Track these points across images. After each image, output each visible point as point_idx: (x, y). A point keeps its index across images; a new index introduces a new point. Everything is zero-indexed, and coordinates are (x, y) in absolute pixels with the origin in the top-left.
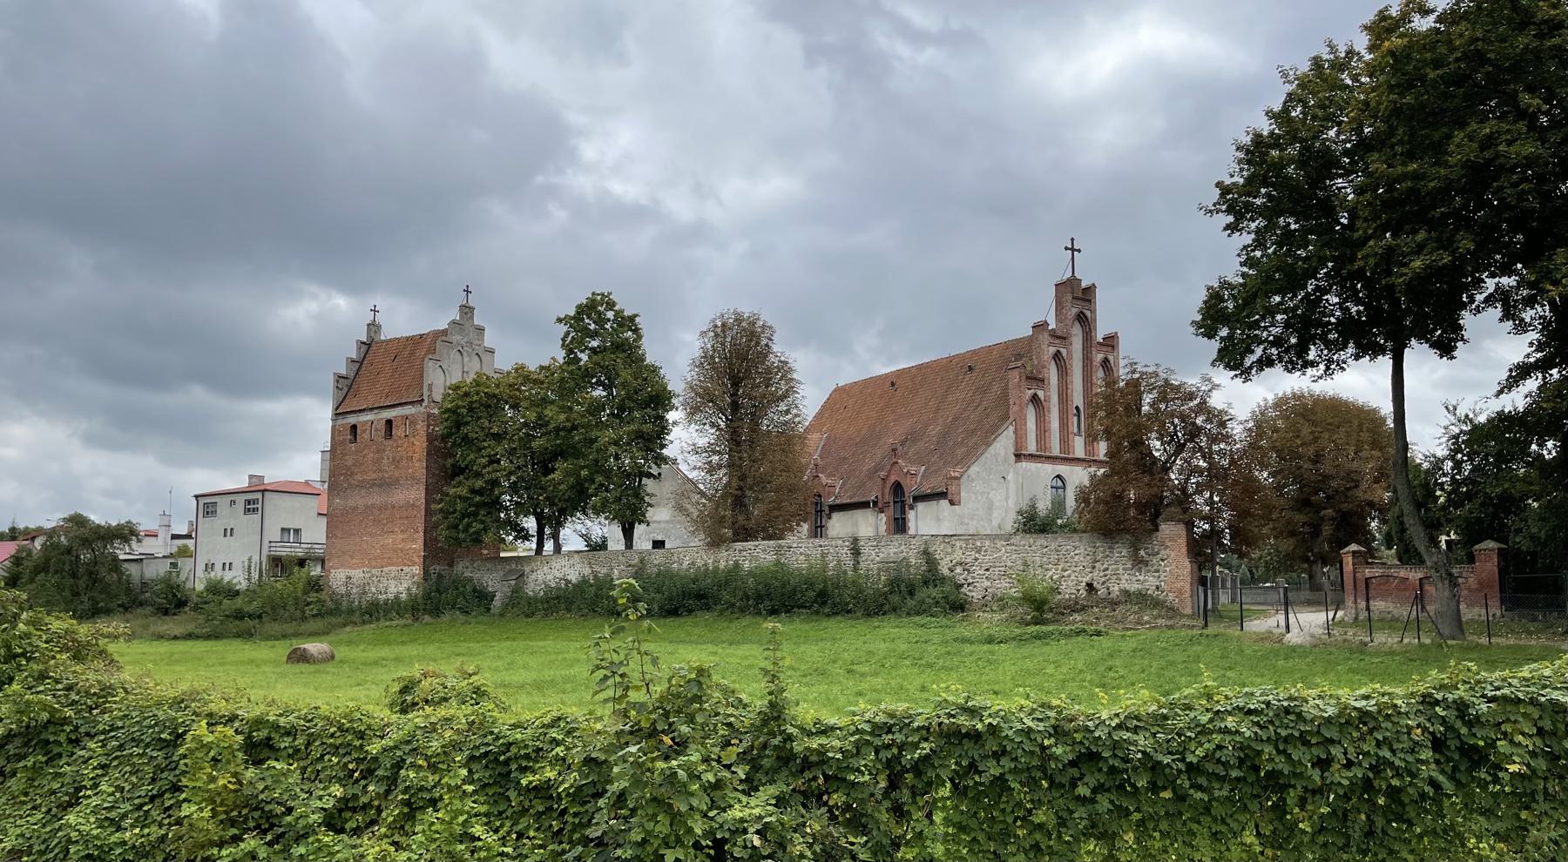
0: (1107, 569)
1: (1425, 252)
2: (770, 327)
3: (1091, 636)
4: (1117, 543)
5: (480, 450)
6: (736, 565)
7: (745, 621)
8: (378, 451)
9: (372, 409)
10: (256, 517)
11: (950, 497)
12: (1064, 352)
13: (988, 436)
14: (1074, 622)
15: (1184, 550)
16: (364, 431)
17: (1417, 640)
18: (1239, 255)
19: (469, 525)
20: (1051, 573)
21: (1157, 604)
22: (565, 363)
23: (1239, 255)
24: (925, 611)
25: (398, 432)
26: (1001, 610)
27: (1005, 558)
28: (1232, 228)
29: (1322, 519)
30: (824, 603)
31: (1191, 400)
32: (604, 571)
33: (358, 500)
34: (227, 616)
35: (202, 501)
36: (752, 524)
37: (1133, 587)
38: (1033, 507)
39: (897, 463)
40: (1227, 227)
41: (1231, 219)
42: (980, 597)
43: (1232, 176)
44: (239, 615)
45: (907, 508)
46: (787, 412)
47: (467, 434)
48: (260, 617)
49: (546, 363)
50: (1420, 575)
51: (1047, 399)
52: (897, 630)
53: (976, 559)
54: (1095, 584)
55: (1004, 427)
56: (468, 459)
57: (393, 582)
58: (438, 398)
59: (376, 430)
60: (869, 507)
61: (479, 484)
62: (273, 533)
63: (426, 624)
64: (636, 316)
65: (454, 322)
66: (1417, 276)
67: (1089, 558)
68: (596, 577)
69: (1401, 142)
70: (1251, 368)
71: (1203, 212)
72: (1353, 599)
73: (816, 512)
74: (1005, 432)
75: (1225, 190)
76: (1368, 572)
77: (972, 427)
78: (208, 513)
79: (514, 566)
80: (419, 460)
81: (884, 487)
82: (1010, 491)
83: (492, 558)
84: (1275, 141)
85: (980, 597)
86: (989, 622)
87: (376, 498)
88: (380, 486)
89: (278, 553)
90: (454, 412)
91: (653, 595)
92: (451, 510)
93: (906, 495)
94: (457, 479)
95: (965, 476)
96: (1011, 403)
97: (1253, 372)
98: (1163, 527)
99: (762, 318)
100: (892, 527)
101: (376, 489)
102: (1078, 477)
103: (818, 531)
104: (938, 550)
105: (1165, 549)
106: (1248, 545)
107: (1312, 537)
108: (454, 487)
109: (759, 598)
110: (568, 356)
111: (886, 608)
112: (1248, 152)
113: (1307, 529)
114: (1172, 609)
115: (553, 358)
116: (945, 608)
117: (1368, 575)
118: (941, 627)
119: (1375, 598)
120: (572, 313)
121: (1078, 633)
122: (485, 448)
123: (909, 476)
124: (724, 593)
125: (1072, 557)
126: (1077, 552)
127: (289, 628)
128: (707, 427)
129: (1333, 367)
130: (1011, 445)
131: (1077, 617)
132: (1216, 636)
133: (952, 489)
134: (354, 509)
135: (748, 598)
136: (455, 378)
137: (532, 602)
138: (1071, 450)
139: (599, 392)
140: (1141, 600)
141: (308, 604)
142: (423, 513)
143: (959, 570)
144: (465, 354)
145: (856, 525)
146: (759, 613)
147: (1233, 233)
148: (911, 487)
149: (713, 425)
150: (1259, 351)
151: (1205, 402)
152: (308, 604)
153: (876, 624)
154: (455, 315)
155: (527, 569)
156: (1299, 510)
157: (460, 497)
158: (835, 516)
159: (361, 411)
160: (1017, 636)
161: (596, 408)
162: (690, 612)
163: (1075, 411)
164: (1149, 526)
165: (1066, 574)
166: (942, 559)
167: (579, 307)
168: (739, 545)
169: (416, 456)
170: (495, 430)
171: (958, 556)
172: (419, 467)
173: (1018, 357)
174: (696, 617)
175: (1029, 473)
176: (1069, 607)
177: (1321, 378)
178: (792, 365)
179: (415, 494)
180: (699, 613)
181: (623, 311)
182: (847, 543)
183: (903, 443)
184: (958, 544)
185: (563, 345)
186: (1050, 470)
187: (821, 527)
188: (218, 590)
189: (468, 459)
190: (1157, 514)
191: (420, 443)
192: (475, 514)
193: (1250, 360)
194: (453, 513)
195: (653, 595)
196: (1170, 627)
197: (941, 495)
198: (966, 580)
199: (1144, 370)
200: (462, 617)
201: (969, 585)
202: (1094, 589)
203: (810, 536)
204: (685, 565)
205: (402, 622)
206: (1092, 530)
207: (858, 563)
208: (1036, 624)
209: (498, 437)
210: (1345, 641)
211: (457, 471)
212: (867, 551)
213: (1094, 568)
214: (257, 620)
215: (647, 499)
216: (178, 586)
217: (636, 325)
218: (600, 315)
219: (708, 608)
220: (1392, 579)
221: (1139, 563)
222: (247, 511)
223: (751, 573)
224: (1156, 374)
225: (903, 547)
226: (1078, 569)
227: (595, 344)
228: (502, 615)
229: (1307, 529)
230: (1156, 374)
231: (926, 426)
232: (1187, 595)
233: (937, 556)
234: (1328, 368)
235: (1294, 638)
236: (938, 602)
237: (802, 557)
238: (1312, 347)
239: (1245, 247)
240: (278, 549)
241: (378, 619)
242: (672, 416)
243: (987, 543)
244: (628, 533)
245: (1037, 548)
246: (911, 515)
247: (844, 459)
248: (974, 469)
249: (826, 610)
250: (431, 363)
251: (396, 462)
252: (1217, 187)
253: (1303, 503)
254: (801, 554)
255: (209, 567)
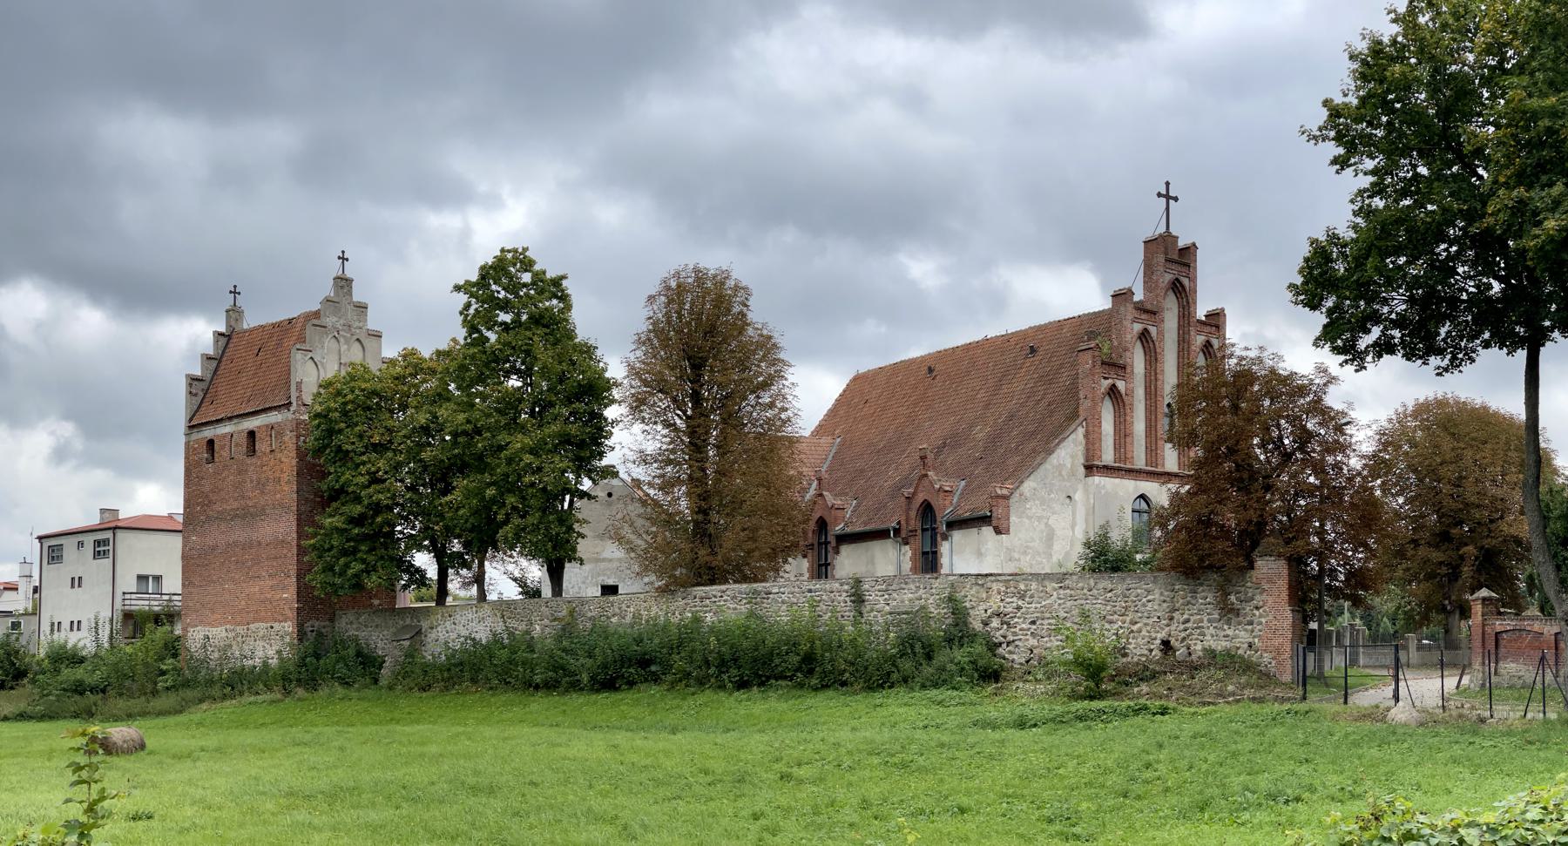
0: (1187, 621)
1: (1561, 209)
2: (745, 289)
3: (1154, 714)
4: (1201, 585)
5: (358, 466)
6: (697, 620)
7: (707, 696)
8: (240, 473)
9: (230, 418)
10: (107, 562)
11: (994, 523)
12: (1153, 330)
13: (1045, 439)
14: (1140, 695)
15: (1285, 595)
16: (223, 447)
17: (1541, 715)
18: (1352, 201)
19: (347, 566)
20: (1116, 626)
21: (1248, 667)
22: (466, 344)
23: (1352, 201)
24: (945, 681)
25: (261, 446)
26: (1049, 678)
27: (1056, 607)
28: (1341, 163)
29: (1462, 558)
30: (811, 672)
31: (1303, 396)
32: (523, 627)
33: (217, 536)
34: (64, 690)
35: (47, 543)
36: (718, 561)
37: (1220, 645)
38: (1105, 536)
39: (926, 475)
40: (1335, 161)
41: (1341, 151)
42: (1023, 661)
43: (1346, 95)
44: (79, 689)
45: (939, 539)
46: (771, 405)
47: (340, 446)
48: (103, 691)
49: (444, 346)
50: (1556, 629)
51: (1130, 392)
52: (906, 709)
53: (1019, 608)
54: (1173, 641)
55: (1071, 429)
56: (343, 479)
57: (261, 643)
58: (308, 400)
59: (236, 445)
60: (889, 537)
61: (358, 509)
62: (128, 583)
63: (299, 699)
64: (564, 277)
65: (328, 300)
66: (1551, 240)
67: (1165, 605)
68: (511, 634)
69: (1542, 68)
70: (1366, 352)
71: (1305, 137)
72: (1480, 659)
73: (820, 544)
74: (1073, 436)
75: (1335, 112)
76: (1499, 625)
77: (1031, 428)
78: (53, 557)
79: (408, 621)
80: (288, 482)
81: (908, 509)
82: (1078, 517)
83: (386, 610)
84: (1398, 53)
85: (1023, 661)
86: (1027, 697)
87: (239, 534)
88: (243, 517)
89: (133, 608)
90: (326, 416)
91: (582, 661)
92: (326, 546)
93: (939, 519)
94: (334, 505)
95: (1017, 494)
96: (1081, 396)
97: (1369, 358)
98: (1259, 563)
99: (734, 275)
100: (919, 565)
101: (238, 521)
102: (1160, 494)
103: (822, 570)
104: (969, 595)
105: (1261, 593)
106: (1366, 588)
107: (1450, 581)
108: (331, 516)
109: (723, 665)
110: (470, 335)
111: (895, 676)
112: (1364, 63)
113: (1444, 570)
114: (1267, 675)
115: (454, 340)
116: (972, 677)
117: (1499, 629)
118: (963, 704)
119: (1506, 658)
120: (474, 277)
121: (1137, 712)
122: (364, 463)
123: (942, 494)
124: (676, 657)
125: (1144, 605)
126: (1150, 597)
127: (137, 704)
128: (659, 427)
129: (1460, 356)
130: (1080, 453)
131: (1144, 688)
132: (1307, 712)
133: (999, 512)
134: (214, 548)
135: (707, 664)
136: (331, 370)
137: (426, 669)
138: (1160, 462)
139: (514, 382)
140: (1229, 663)
141: (163, 673)
142: (295, 551)
143: (995, 623)
144: (342, 340)
145: (872, 562)
146: (722, 687)
147: (1342, 169)
148: (946, 510)
149: (668, 424)
150: (1376, 332)
151: (1320, 400)
152: (163, 673)
153: (878, 702)
154: (327, 289)
155: (425, 625)
156: (1437, 547)
157: (337, 528)
158: (846, 550)
159: (218, 421)
160: (1058, 716)
161: (511, 403)
162: (631, 684)
163: (1166, 410)
164: (1241, 562)
165: (1135, 628)
166: (973, 608)
167: (482, 268)
168: (700, 591)
169: (285, 477)
170: (376, 439)
171: (994, 603)
172: (287, 490)
173: (1092, 335)
174: (639, 691)
175: (1103, 492)
176: (1136, 674)
177: (1446, 370)
178: (777, 339)
179: (282, 527)
180: (643, 686)
181: (544, 273)
182: (846, 587)
183: (939, 450)
184: (995, 586)
185: (465, 321)
186: (1128, 488)
187: (827, 565)
188: (65, 658)
189: (343, 479)
190: (1255, 545)
191: (289, 461)
192: (355, 551)
193: (1365, 341)
194: (329, 550)
195: (582, 661)
196: (1260, 700)
197: (984, 520)
198: (1005, 637)
199: (1244, 354)
200: (340, 691)
201: (1009, 644)
202: (1171, 648)
203: (812, 577)
204: (628, 619)
205: (268, 696)
206: (1173, 568)
207: (861, 614)
208: (1092, 698)
209: (379, 448)
210: (1460, 716)
211: (337, 494)
212: (873, 597)
213: (1171, 619)
214: (101, 695)
215: (576, 526)
216: (17, 652)
217: (563, 291)
218: (511, 278)
219: (656, 679)
220: (1524, 633)
221: (1228, 612)
222: (97, 555)
223: (712, 630)
224: (1260, 360)
225: (922, 591)
226: (1150, 621)
227: (505, 317)
228: (391, 688)
229: (1444, 570)
230: (1260, 360)
231: (971, 426)
232: (1287, 655)
233: (967, 605)
234: (1454, 358)
235: (1400, 713)
236: (963, 669)
237: (784, 607)
238: (1448, 324)
239: (1361, 192)
240: (133, 602)
241: (241, 693)
242: (611, 413)
243: (1034, 586)
244: (556, 574)
245: (1103, 592)
246: (944, 548)
247: (862, 471)
248: (1028, 486)
249: (814, 681)
250: (299, 355)
251: (261, 485)
252: (1325, 106)
253: (1443, 538)
254: (783, 602)
255: (56, 627)
